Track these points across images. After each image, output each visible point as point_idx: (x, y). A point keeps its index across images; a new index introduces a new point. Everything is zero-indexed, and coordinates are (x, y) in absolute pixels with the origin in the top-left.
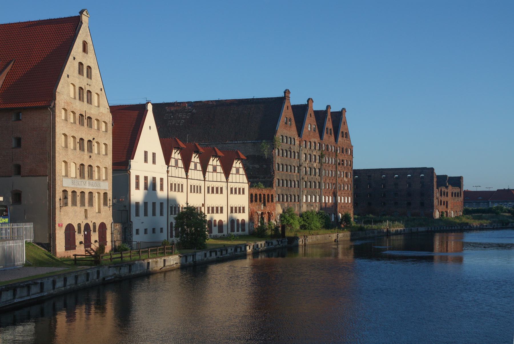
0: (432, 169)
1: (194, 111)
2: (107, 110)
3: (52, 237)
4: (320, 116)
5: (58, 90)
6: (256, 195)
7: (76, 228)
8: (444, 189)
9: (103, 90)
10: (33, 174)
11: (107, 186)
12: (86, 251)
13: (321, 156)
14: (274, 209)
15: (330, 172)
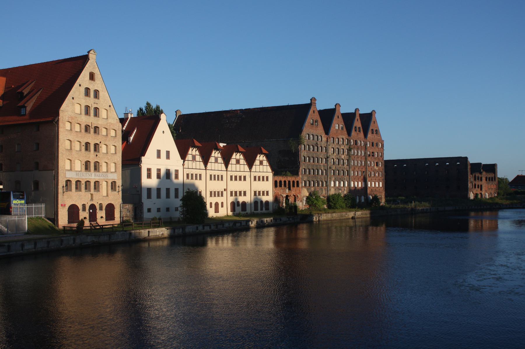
0: (466, 158)
1: (244, 116)
2: (116, 121)
3: (56, 214)
4: (348, 119)
5: (61, 108)
6: (289, 182)
7: (80, 208)
8: (477, 175)
9: (112, 106)
10: (46, 169)
11: (117, 176)
12: (91, 224)
13: (349, 150)
14: (300, 192)
15: (360, 162)
